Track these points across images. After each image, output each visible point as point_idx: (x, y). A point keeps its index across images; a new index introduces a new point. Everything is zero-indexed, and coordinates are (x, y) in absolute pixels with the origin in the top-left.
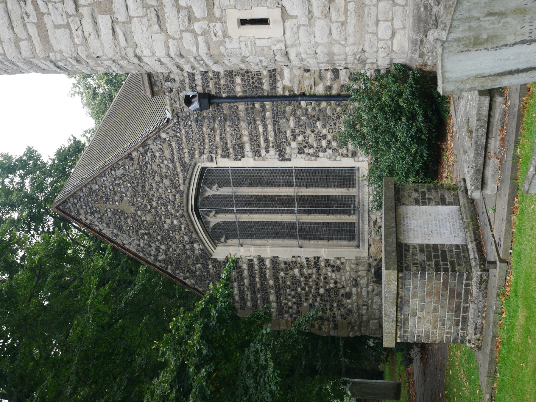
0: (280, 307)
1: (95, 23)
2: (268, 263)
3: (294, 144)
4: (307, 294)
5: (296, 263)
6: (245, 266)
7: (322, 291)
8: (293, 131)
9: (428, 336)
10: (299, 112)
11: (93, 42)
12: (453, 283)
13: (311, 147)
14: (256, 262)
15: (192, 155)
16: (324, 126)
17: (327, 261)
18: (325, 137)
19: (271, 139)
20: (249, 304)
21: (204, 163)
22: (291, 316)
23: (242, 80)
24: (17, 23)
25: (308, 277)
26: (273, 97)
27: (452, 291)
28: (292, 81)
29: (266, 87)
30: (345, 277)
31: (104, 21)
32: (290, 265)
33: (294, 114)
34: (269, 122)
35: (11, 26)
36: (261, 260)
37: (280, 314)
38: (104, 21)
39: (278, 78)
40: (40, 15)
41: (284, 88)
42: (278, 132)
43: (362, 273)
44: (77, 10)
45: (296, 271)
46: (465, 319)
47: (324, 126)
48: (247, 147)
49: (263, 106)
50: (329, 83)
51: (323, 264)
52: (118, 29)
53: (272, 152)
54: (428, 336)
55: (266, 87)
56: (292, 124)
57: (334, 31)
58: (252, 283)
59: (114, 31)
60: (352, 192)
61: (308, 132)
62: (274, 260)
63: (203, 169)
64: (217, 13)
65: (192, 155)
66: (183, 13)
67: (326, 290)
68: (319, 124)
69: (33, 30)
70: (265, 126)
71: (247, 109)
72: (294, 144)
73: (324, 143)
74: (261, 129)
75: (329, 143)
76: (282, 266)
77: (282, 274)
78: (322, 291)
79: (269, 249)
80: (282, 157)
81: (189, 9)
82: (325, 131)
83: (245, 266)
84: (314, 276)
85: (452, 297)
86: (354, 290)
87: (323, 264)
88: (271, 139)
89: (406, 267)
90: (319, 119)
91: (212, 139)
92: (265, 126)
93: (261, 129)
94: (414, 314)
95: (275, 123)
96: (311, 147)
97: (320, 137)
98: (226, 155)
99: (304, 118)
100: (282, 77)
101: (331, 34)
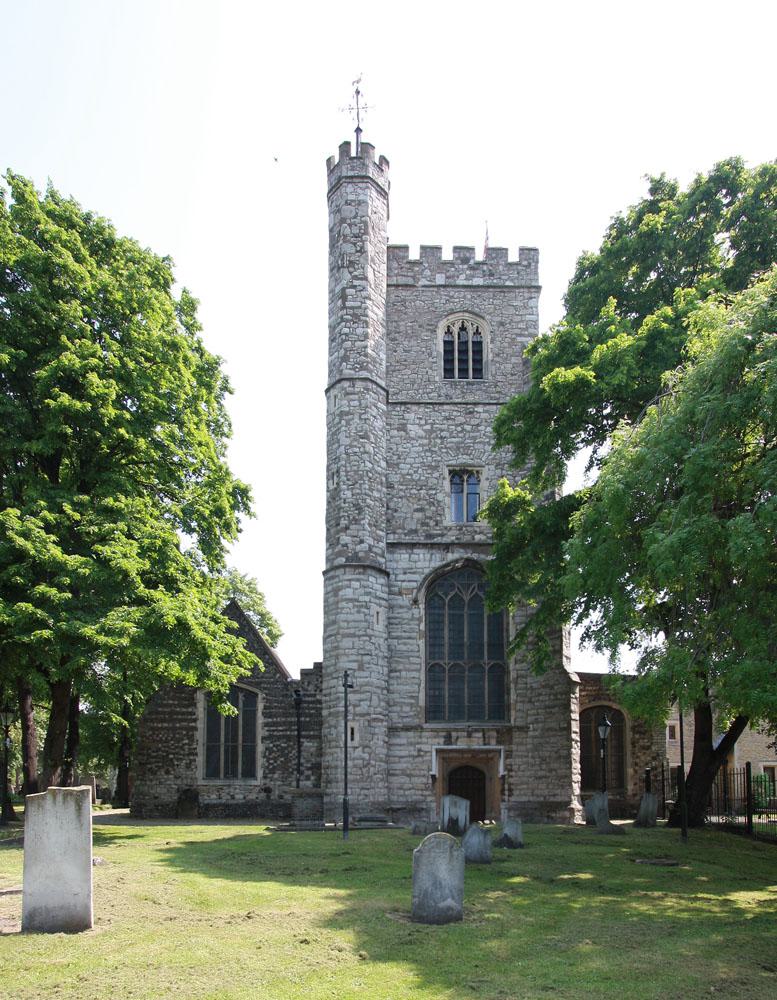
0: (158, 729)
2: (193, 724)
3: (271, 745)
4: (168, 747)
5: (193, 741)
6: (190, 710)
7: (171, 756)
11: (345, 659)
13: (270, 754)
14: (194, 717)
15: (265, 688)
17: (195, 760)
19: (275, 733)
20: (160, 709)
21: (261, 696)
22: (151, 735)
24: (357, 624)
25: (182, 748)
26: (299, 736)
29: (303, 733)
30: (182, 770)
32: (191, 738)
33: (289, 746)
34: (284, 733)
35: (355, 621)
36: (195, 720)
37: (152, 729)
40: (359, 636)
42: (279, 738)
43: (185, 782)
45: (187, 741)
48: (270, 720)
49: (295, 730)
51: (192, 758)
53: (267, 733)
55: (303, 733)
58: (178, 713)
60: (240, 776)
62: (196, 729)
63: (257, 695)
64: (357, 718)
65: (265, 688)
66: (357, 702)
67: (172, 759)
69: (352, 631)
70: (282, 731)
72: (271, 745)
73: (271, 761)
74: (280, 728)
76: (191, 733)
77: (184, 732)
78: (171, 756)
79: (202, 726)
80: (263, 739)
81: (359, 705)
82: (279, 762)
83: (190, 710)
84: (182, 752)
86: (171, 776)
87: (192, 758)
88: (275, 733)
89: (590, 796)
91: (276, 701)
92: (282, 731)
93: (280, 728)
96: (270, 754)
97: (275, 759)
98: (265, 708)
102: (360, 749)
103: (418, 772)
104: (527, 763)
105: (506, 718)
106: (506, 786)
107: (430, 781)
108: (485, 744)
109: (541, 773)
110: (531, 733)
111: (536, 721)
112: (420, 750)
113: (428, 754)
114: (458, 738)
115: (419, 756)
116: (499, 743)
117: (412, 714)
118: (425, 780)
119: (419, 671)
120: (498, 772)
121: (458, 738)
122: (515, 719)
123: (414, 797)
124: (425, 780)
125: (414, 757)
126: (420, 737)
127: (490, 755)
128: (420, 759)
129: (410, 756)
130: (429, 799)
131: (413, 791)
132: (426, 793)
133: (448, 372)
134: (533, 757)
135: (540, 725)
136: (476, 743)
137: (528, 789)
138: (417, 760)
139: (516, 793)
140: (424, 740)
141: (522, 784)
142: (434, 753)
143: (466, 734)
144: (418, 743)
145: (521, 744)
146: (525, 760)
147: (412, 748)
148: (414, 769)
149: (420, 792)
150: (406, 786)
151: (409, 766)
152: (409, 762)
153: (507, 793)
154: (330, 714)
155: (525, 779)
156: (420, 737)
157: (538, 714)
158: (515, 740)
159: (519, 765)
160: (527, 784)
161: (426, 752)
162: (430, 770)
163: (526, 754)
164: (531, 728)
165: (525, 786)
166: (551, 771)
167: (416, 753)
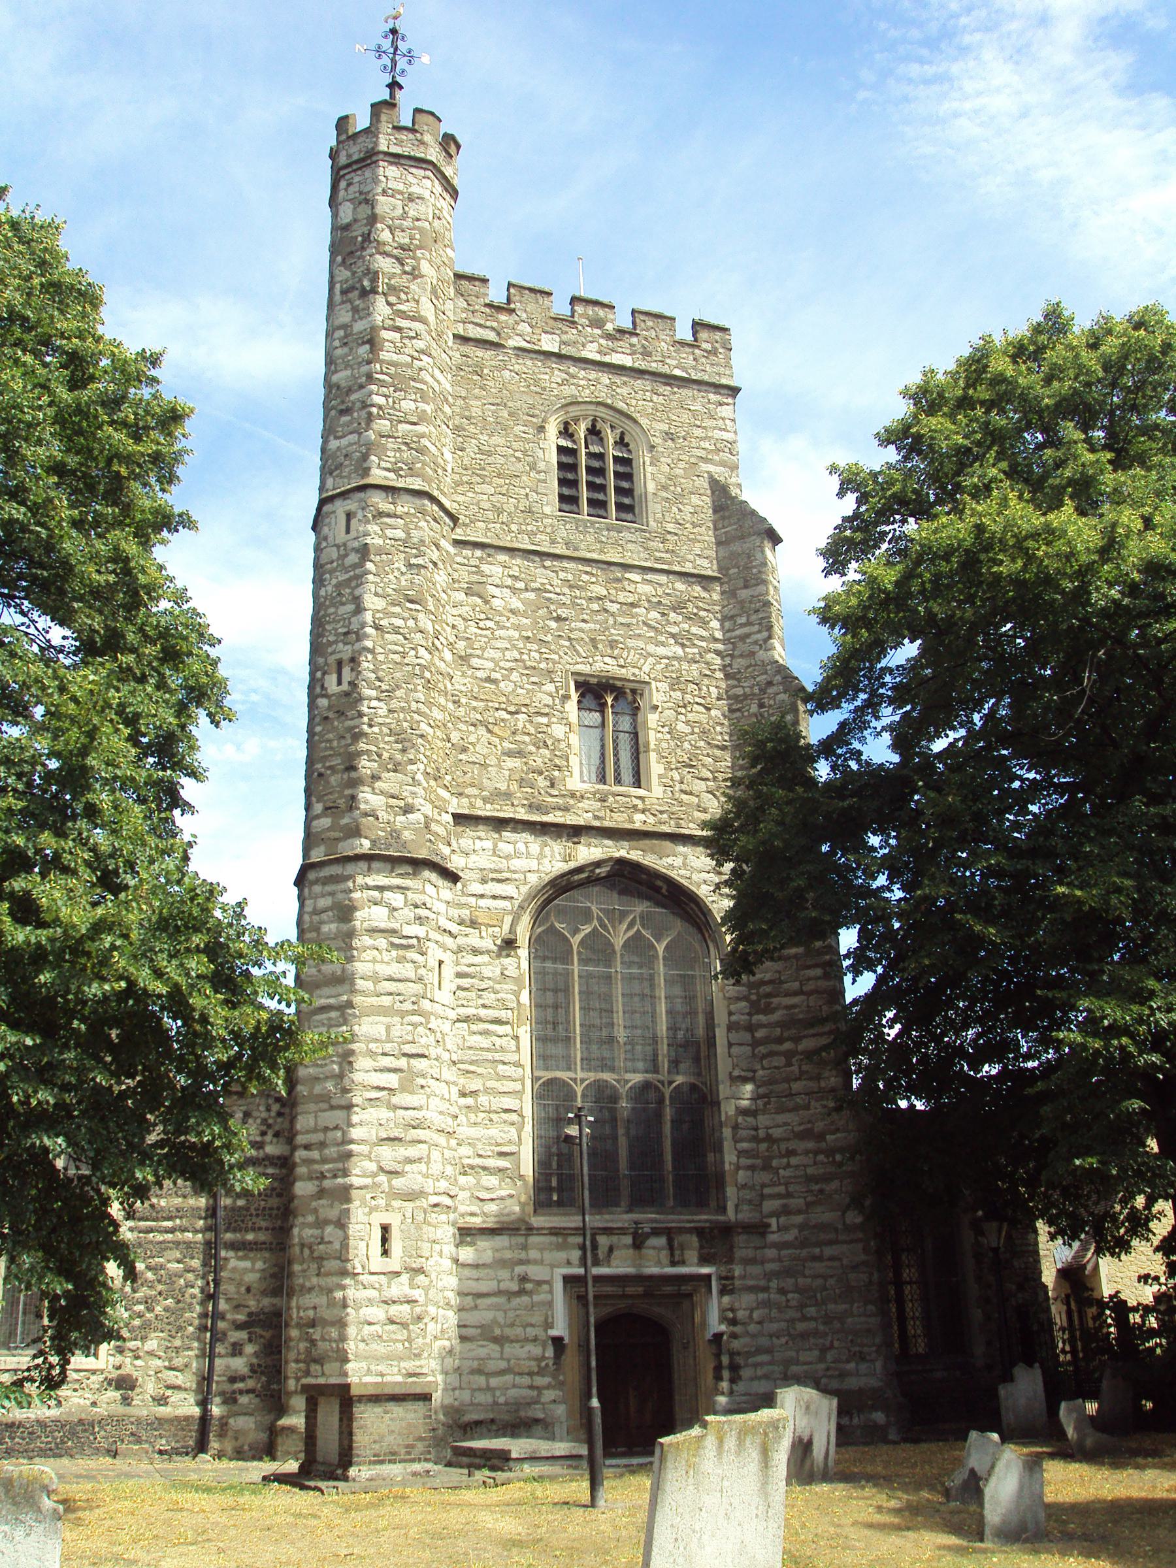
1: (390, 1070)
8: (162, 1267)
9: (361, 1427)
10: (190, 1276)
12: (420, 1446)
16: (166, 1309)
18: (150, 1309)
23: (240, 1208)
27: (412, 1446)
28: (234, 1270)
31: (392, 1080)
38: (392, 1080)
39: (240, 1254)
41: (226, 1259)
44: (405, 1055)
46: (382, 1462)
47: (166, 1309)
50: (229, 1316)
52: (385, 1093)
54: (361, 1427)
56: (174, 1266)
57: (373, 1328)
59: (384, 1089)
61: (160, 1287)
68: (170, 1302)
70: (171, 1231)
71: (199, 1208)
73: (140, 1308)
74: (169, 1224)
75: (140, 1315)
82: (158, 1309)
85: (407, 1446)
90: (179, 1302)
92: (171, 1231)
93: (169, 1224)
94: (386, 1412)
95: (177, 1244)
99: (182, 1281)
100: (239, 1259)
101: (370, 1324)
102: (405, 1278)
103: (519, 1331)
104: (767, 1304)
105: (713, 1204)
106: (725, 1360)
107: (550, 1352)
108: (673, 1264)
109: (801, 1326)
110: (773, 1238)
111: (786, 1211)
112: (524, 1279)
113: (546, 1287)
114: (611, 1250)
115: (521, 1292)
116: (704, 1260)
117: (504, 1193)
118: (537, 1351)
119: (518, 1094)
120: (704, 1323)
121: (611, 1250)
122: (737, 1206)
123: (513, 1392)
124: (537, 1351)
125: (510, 1295)
126: (525, 1247)
127: (686, 1288)
128: (525, 1299)
129: (499, 1293)
130: (549, 1395)
131: (509, 1378)
132: (540, 1381)
133: (568, 501)
134: (782, 1291)
135: (798, 1219)
136: (655, 1264)
137: (770, 1363)
138: (517, 1301)
139: (746, 1373)
140: (533, 1254)
141: (759, 1351)
142: (559, 1286)
143: (628, 1240)
144: (521, 1262)
145: (752, 1261)
146: (762, 1296)
147: (504, 1274)
148: (512, 1325)
149: (526, 1380)
150: (492, 1366)
151: (500, 1316)
152: (496, 1307)
153: (726, 1374)
154: (321, 1193)
155: (764, 1341)
156: (525, 1247)
157: (789, 1195)
158: (739, 1254)
159: (752, 1311)
160: (769, 1351)
161: (539, 1283)
162: (548, 1325)
163: (762, 1283)
164: (774, 1227)
165: (764, 1358)
166: (828, 1319)
167: (515, 1287)
